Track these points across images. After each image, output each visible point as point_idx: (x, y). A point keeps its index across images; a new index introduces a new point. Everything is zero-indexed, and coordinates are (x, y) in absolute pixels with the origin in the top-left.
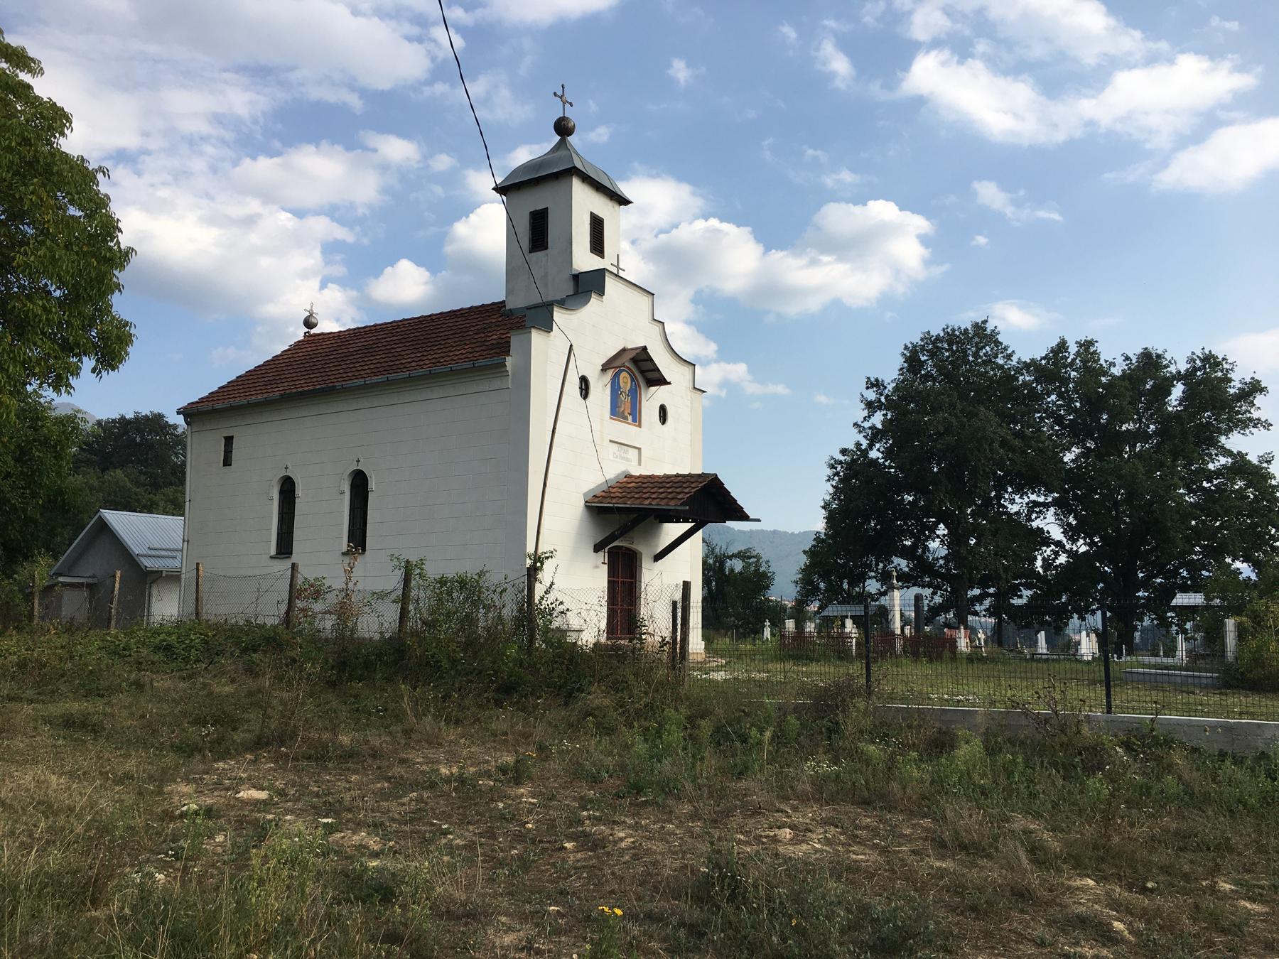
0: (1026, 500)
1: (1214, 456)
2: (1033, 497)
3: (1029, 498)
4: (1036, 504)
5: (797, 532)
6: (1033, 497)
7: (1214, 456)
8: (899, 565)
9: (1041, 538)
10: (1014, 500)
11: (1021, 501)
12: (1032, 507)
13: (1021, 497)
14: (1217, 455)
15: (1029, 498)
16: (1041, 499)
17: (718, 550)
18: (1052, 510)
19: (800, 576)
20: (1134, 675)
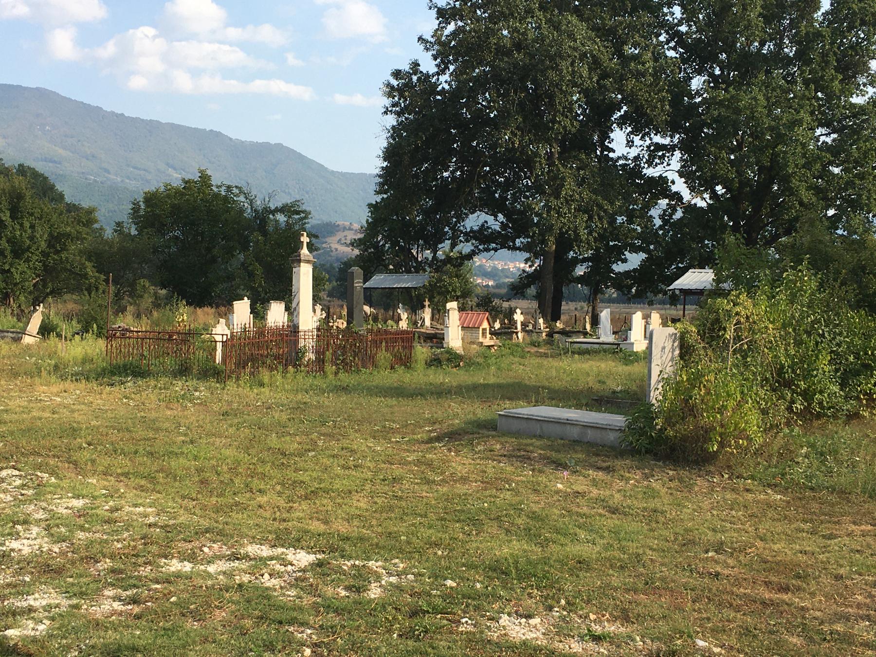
0: (648, 142)
1: (862, 87)
2: (658, 139)
3: (651, 139)
4: (659, 147)
5: (107, 108)
6: (658, 139)
7: (862, 87)
8: (486, 222)
9: (660, 186)
10: (633, 142)
11: (642, 143)
12: (653, 151)
13: (642, 138)
14: (865, 85)
15: (651, 139)
16: (666, 141)
17: (258, 203)
18: (678, 154)
19: (361, 236)
20: (682, 312)
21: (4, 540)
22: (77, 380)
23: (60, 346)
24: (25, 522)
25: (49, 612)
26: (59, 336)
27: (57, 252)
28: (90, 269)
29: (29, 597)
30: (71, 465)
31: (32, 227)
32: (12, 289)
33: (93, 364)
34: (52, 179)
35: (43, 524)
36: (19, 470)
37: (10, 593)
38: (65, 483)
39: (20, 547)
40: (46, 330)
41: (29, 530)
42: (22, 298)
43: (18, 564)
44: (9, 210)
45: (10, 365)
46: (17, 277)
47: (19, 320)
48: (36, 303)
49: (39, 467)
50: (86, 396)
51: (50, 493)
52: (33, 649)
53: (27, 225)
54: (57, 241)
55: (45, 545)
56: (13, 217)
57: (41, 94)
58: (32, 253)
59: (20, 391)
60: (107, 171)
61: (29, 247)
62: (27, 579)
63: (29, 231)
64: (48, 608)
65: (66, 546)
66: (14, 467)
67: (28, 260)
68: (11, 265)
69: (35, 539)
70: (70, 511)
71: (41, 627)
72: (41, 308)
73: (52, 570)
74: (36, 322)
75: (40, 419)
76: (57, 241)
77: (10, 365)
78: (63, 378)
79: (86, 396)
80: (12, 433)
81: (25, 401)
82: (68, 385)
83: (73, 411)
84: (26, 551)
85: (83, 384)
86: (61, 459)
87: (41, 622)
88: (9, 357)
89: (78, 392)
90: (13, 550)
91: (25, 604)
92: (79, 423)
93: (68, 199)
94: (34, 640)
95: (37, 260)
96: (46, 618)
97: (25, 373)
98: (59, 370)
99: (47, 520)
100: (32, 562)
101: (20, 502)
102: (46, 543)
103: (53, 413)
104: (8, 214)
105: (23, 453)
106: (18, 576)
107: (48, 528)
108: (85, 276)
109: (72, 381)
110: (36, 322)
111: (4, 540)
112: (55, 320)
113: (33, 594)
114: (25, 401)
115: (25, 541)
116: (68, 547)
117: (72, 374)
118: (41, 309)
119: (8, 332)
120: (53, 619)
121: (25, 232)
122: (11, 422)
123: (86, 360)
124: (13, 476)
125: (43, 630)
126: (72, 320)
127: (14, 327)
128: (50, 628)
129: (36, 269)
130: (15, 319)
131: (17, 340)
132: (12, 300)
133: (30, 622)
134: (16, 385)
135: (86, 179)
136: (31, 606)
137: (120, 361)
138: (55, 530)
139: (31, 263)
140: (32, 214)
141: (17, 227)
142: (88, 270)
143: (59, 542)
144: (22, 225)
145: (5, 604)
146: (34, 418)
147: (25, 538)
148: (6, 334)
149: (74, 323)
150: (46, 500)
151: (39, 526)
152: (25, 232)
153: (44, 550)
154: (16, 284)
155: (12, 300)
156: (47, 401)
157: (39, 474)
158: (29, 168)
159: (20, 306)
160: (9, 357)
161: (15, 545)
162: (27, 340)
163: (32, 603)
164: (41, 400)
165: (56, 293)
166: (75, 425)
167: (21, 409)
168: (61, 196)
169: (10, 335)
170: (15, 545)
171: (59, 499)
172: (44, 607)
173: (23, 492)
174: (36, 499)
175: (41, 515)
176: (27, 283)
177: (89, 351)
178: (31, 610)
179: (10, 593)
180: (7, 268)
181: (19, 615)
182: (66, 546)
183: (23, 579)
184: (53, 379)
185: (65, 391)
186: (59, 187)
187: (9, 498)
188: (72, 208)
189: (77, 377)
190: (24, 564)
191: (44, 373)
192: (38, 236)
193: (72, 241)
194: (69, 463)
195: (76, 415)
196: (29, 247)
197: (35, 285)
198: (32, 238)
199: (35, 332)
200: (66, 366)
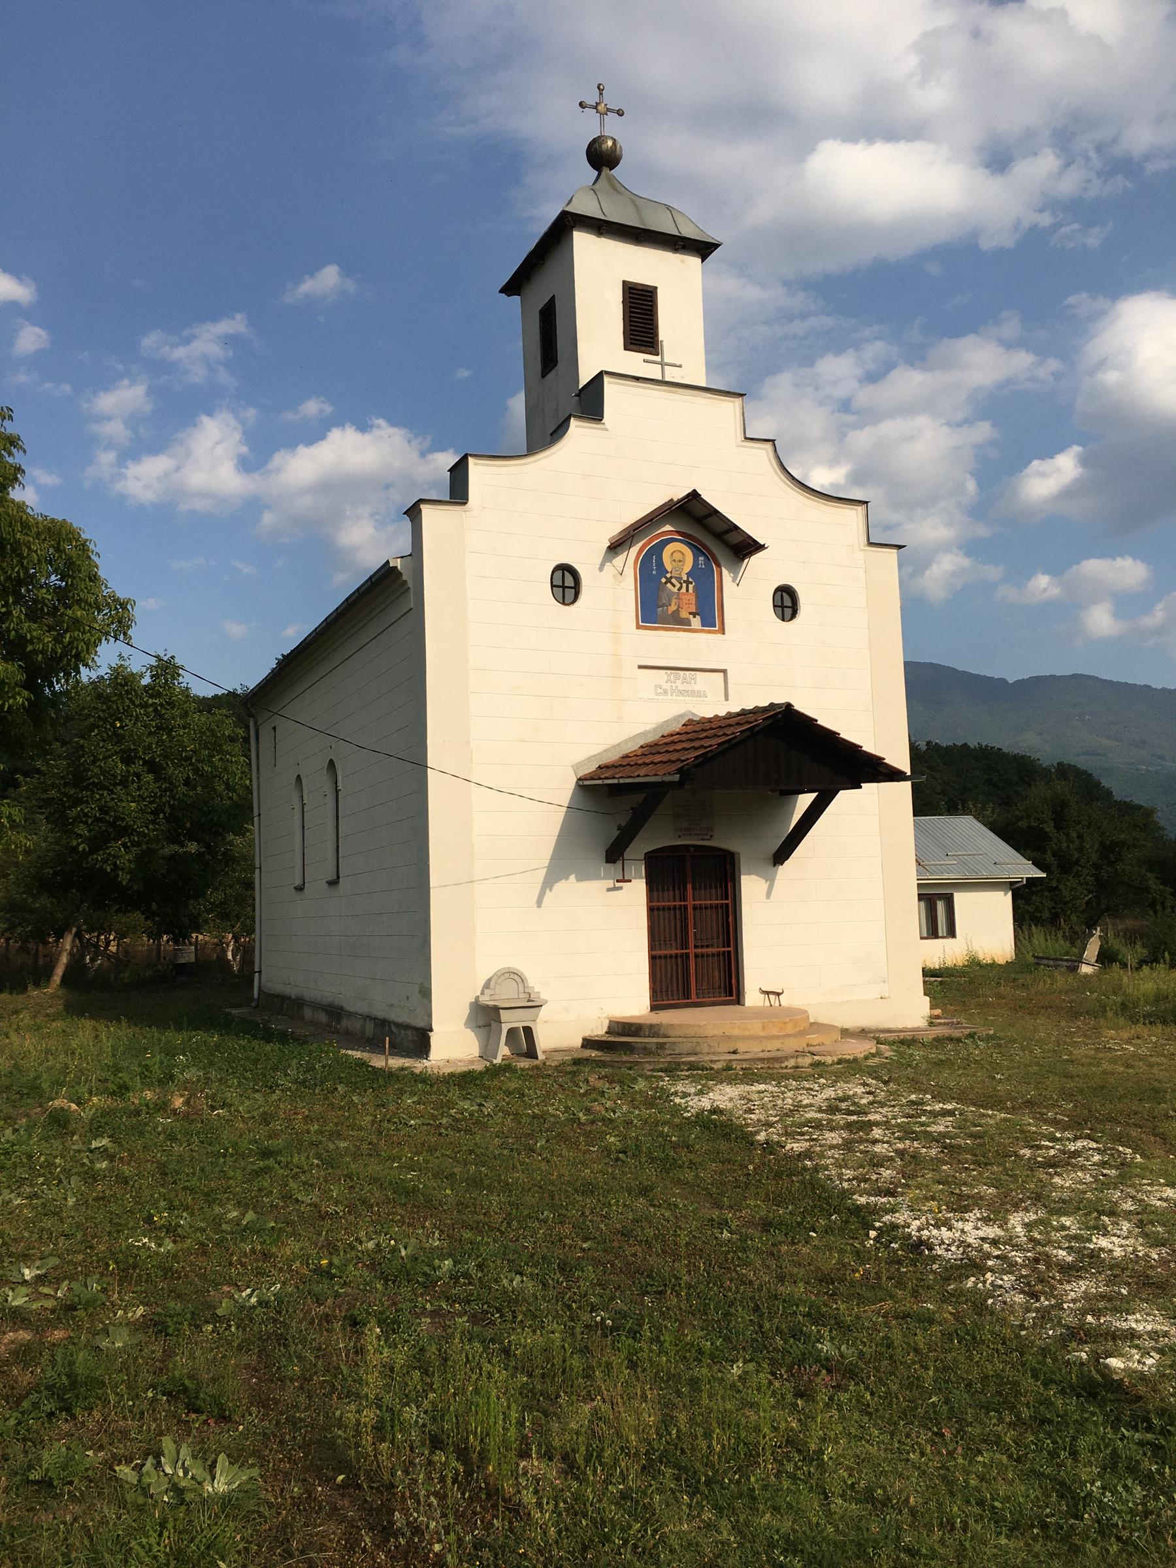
21: (1091, 1235)
22: (1151, 1023)
23: (1125, 979)
24: (1112, 1213)
25: (1157, 1341)
26: (1124, 965)
27: (1111, 863)
28: (1152, 881)
29: (1130, 1317)
30: (1158, 1139)
31: (1080, 837)
32: (1061, 908)
33: (1169, 1002)
34: (1096, 774)
35: (1135, 1219)
36: (1097, 1142)
37: (1106, 1308)
38: (1155, 1164)
39: (1110, 1246)
40: (1106, 957)
41: (1118, 1224)
42: (1074, 918)
43: (1110, 1269)
44: (1053, 819)
45: (1068, 1002)
46: (1067, 895)
47: (1072, 943)
48: (1091, 924)
49: (1119, 1139)
50: (1165, 1045)
51: (1137, 1176)
52: (1142, 1389)
53: (1074, 835)
54: (1110, 851)
55: (1140, 1248)
56: (1058, 827)
57: (1078, 680)
58: (1082, 867)
59: (1085, 1036)
60: (1161, 758)
61: (1078, 860)
62: (1124, 1292)
63: (1077, 841)
64: (1154, 1335)
65: (1166, 1252)
66: (1089, 1137)
67: (1077, 875)
68: (1059, 882)
69: (1127, 1238)
70: (1165, 1204)
71: (1150, 1361)
72: (1098, 932)
73: (1153, 1283)
74: (1092, 949)
75: (1113, 1074)
76: (1110, 851)
77: (1068, 1002)
78: (1134, 1020)
79: (1165, 1045)
80: (1081, 1091)
81: (1091, 1049)
82: (1139, 1029)
83: (1151, 1065)
84: (1118, 1253)
85: (1159, 1028)
86: (1144, 1129)
87: (1148, 1354)
88: (1066, 993)
89: (1154, 1039)
90: (1101, 1249)
91: (1125, 1325)
92: (1160, 1082)
93: (1117, 796)
94: (1142, 1377)
95: (1088, 875)
96: (1154, 1349)
97: (1087, 1013)
98: (1128, 1010)
99: (1138, 1214)
100: (1127, 1269)
101: (1104, 1185)
102: (1141, 1245)
103: (1127, 1067)
104: (1052, 824)
105: (1097, 1119)
106: (1113, 1285)
107: (1141, 1224)
108: (1147, 890)
109: (1144, 1024)
110: (1092, 949)
111: (1091, 1235)
112: (1116, 944)
113: (1134, 1313)
114: (1091, 1049)
115: (1114, 1239)
116: (1168, 1254)
117: (1144, 1016)
118: (1098, 934)
119: (1062, 960)
120: (1161, 1351)
121: (1073, 842)
122: (1078, 1076)
123: (1159, 998)
124: (1090, 1149)
125: (1152, 1365)
126: (1135, 943)
127: (1067, 954)
128: (1159, 1364)
129: (1087, 884)
130: (1068, 943)
131: (1074, 969)
132: (1062, 920)
133: (1134, 1351)
134: (1078, 1027)
135: (1137, 770)
136: (1133, 1329)
137: (612, 190)
138: (1150, 1228)
139: (1081, 879)
140: (1079, 823)
141: (1063, 838)
142: (1150, 882)
143: (1157, 1246)
144: (1068, 835)
145: (1102, 1321)
146: (1105, 1072)
147: (1114, 1235)
148: (1060, 963)
149: (1138, 947)
150: (1133, 1186)
151: (1130, 1221)
152: (1073, 842)
153: (1140, 1254)
154: (1066, 903)
155: (1062, 920)
156: (1118, 1050)
157: (1121, 1149)
158: (1069, 765)
159: (1072, 928)
160: (1066, 993)
161: (1104, 1243)
162: (1085, 969)
163: (1134, 1325)
164: (1110, 1048)
165: (1113, 911)
166: (1156, 1084)
167: (1088, 1060)
168: (1109, 793)
169: (1065, 963)
170: (1104, 1243)
171: (1149, 1185)
172: (1149, 1333)
173: (1105, 1171)
174: (1121, 1183)
175: (1128, 1206)
176: (1078, 901)
177: (1163, 987)
178: (1132, 1335)
179: (1106, 1308)
180: (1054, 885)
181: (1120, 1339)
182: (1166, 1252)
183: (1120, 1291)
184: (1122, 1021)
185: (1138, 1038)
186: (1105, 783)
187: (1089, 1179)
188: (1127, 808)
189: (1151, 1019)
190: (1117, 1270)
191: (1110, 1014)
192: (1088, 846)
193: (1128, 849)
194: (1156, 1135)
195: (1155, 1070)
196: (1078, 860)
197: (1088, 903)
198: (1081, 850)
199: (1093, 960)
200: (1135, 1004)
